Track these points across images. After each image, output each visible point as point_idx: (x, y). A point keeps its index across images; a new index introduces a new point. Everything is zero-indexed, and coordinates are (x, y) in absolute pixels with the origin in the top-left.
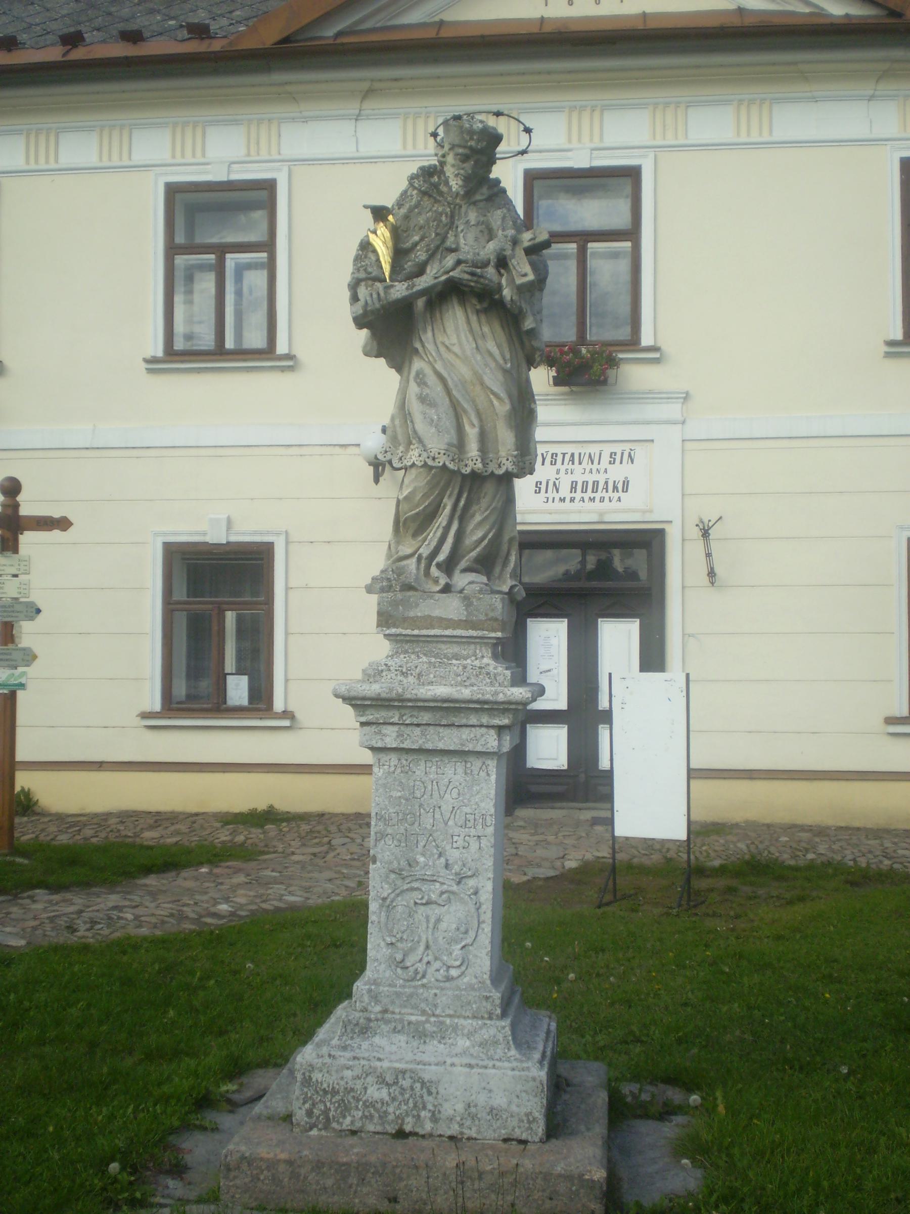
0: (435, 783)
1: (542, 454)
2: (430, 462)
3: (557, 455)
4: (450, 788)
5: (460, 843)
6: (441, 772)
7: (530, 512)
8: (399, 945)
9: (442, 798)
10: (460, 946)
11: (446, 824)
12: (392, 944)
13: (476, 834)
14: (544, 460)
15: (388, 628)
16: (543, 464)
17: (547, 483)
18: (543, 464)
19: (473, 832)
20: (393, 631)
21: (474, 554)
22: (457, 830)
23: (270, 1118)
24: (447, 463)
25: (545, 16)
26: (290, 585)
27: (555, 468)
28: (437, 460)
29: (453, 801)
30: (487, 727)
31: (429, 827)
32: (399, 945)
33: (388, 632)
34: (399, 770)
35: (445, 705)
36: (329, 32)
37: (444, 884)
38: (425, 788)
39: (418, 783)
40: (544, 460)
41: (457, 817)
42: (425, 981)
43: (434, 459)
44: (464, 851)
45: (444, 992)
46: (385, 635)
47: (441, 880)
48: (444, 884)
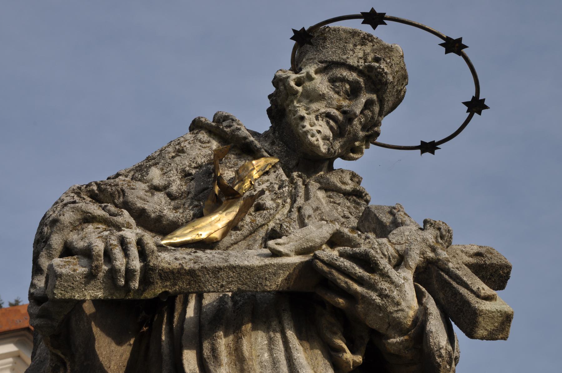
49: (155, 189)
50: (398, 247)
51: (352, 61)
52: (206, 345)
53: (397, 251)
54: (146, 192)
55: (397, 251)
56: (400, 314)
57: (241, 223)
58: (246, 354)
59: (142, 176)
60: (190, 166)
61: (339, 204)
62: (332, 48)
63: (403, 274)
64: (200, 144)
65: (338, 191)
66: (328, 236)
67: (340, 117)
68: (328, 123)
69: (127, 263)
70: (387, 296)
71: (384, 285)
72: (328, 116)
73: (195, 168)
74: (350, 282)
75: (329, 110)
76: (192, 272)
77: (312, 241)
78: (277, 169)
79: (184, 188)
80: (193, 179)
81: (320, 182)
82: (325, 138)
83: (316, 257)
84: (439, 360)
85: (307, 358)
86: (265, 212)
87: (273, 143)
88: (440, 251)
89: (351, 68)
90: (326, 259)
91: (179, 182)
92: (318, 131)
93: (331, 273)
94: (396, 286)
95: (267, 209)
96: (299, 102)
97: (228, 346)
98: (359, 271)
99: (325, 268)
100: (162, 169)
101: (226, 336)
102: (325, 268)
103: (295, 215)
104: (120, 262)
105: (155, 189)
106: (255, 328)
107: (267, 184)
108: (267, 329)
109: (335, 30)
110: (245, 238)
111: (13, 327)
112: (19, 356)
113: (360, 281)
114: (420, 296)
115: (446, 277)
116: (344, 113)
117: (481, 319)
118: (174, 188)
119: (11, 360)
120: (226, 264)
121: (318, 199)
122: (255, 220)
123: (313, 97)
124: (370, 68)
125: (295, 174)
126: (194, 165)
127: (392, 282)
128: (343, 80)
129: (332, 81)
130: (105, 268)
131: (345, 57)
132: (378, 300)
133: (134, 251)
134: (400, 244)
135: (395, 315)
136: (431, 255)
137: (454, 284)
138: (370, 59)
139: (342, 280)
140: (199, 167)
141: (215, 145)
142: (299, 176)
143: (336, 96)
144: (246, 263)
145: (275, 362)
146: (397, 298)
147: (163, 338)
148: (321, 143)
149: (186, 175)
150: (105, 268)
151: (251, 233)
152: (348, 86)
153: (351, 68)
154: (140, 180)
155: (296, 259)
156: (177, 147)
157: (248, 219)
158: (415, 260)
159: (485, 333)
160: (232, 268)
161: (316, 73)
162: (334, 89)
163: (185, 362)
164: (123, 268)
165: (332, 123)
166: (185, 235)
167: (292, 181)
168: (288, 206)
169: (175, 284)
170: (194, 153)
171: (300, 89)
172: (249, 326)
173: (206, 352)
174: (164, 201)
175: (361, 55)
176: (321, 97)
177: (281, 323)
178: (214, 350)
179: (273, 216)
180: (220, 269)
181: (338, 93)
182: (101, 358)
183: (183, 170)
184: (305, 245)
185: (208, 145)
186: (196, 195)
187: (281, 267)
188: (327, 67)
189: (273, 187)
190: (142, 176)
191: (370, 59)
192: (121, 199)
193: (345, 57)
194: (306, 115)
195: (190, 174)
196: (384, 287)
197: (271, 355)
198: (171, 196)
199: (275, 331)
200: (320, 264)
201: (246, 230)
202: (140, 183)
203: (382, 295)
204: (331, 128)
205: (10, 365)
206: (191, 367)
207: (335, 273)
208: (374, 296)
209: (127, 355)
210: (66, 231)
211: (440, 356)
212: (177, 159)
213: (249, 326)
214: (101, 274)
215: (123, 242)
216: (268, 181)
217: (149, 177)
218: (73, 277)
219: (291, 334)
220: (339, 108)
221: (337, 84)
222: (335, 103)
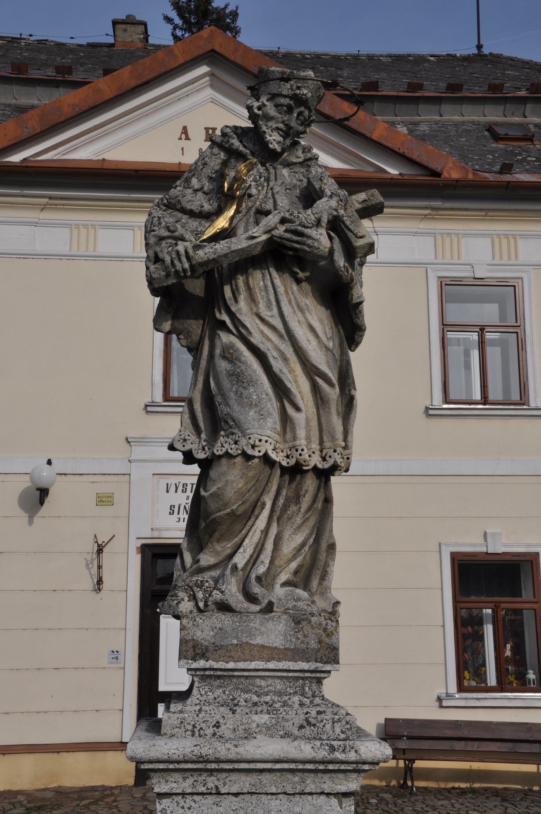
1: (176, 484)
2: (250, 452)
3: (187, 485)
7: (167, 529)
14: (177, 488)
15: (194, 659)
16: (176, 492)
17: (179, 507)
18: (176, 492)
20: (202, 663)
21: (294, 565)
24: (270, 452)
25: (182, 162)
27: (185, 495)
28: (257, 449)
30: (328, 794)
33: (195, 665)
35: (278, 766)
36: (16, 158)
40: (177, 488)
43: (253, 447)
46: (189, 670)
49: (196, 191)
50: (316, 216)
51: (285, 92)
52: (233, 282)
53: (316, 218)
54: (192, 194)
55: (316, 218)
56: (321, 253)
57: (240, 209)
58: (252, 286)
59: (188, 185)
60: (211, 173)
61: (296, 173)
62: (273, 84)
63: (320, 231)
64: (214, 157)
65: (295, 164)
66: (278, 221)
67: (284, 129)
68: (279, 133)
69: (182, 266)
70: (312, 247)
71: (310, 242)
72: (277, 128)
73: (214, 173)
74: (293, 244)
75: (277, 125)
76: (214, 260)
77: (270, 226)
78: (257, 165)
79: (211, 187)
80: (214, 180)
81: (283, 165)
82: (279, 143)
83: (273, 236)
84: (341, 273)
85: (281, 281)
86: (252, 198)
87: (254, 144)
88: (339, 211)
89: (285, 96)
90: (278, 235)
91: (207, 184)
92: (274, 140)
93: (282, 242)
94: (316, 240)
95: (253, 196)
96: (262, 121)
97: (243, 281)
98: (295, 238)
99: (279, 240)
100: (198, 178)
101: (242, 276)
102: (279, 240)
103: (270, 195)
104: (179, 267)
105: (196, 191)
106: (255, 269)
107: (253, 177)
108: (261, 268)
109: (272, 72)
110: (244, 216)
111: (202, 52)
112: (213, 74)
113: (297, 242)
114: (331, 238)
115: (343, 226)
116: (286, 125)
117: (357, 250)
118: (206, 188)
119: (207, 78)
120: (229, 251)
121: (284, 176)
122: (248, 205)
123: (268, 118)
124: (295, 95)
125: (268, 165)
126: (213, 171)
127: (313, 239)
128: (282, 105)
129: (276, 106)
130: (173, 270)
131: (280, 90)
132: (308, 249)
133: (184, 259)
134: (317, 213)
135: (318, 253)
136: (335, 213)
137: (346, 230)
138: (294, 88)
139: (288, 243)
140: (217, 172)
141: (222, 155)
142: (270, 165)
143: (280, 115)
144: (240, 247)
145: (266, 286)
146: (317, 246)
147: (216, 276)
148: (277, 146)
149: (210, 178)
150: (173, 270)
151: (247, 212)
152: (285, 108)
153: (285, 96)
154: (188, 188)
155: (264, 237)
156: (203, 162)
157: (244, 205)
158: (325, 220)
159: (362, 255)
160: (233, 252)
161: (267, 100)
162: (278, 112)
163: (225, 293)
164: (181, 269)
165: (280, 132)
166: (210, 232)
167: (267, 169)
168: (265, 188)
169: (207, 267)
170: (212, 164)
171: (260, 112)
172: (251, 269)
173: (234, 287)
174: (202, 197)
175: (289, 87)
176: (271, 118)
177: (267, 263)
178: (236, 286)
179: (258, 198)
180: (227, 254)
181: (280, 113)
182: (190, 291)
183: (209, 176)
184: (267, 229)
185: (219, 156)
186: (217, 191)
187: (258, 243)
188: (273, 97)
189: (256, 178)
190: (188, 185)
191: (294, 88)
192: (180, 206)
193: (280, 90)
194: (266, 130)
195: (213, 178)
196: (309, 243)
197: (264, 283)
198: (204, 193)
199: (264, 269)
200: (276, 238)
201: (244, 211)
202: (188, 190)
203: (309, 246)
204: (281, 136)
205: (209, 82)
206: (228, 295)
207: (284, 241)
208: (306, 248)
209: (203, 282)
210: (153, 248)
211: (341, 271)
212: (204, 170)
213: (251, 269)
214: (172, 273)
215: (178, 253)
216: (253, 174)
217: (192, 184)
218: (160, 278)
219: (272, 270)
220: (283, 122)
221: (279, 108)
222: (280, 120)
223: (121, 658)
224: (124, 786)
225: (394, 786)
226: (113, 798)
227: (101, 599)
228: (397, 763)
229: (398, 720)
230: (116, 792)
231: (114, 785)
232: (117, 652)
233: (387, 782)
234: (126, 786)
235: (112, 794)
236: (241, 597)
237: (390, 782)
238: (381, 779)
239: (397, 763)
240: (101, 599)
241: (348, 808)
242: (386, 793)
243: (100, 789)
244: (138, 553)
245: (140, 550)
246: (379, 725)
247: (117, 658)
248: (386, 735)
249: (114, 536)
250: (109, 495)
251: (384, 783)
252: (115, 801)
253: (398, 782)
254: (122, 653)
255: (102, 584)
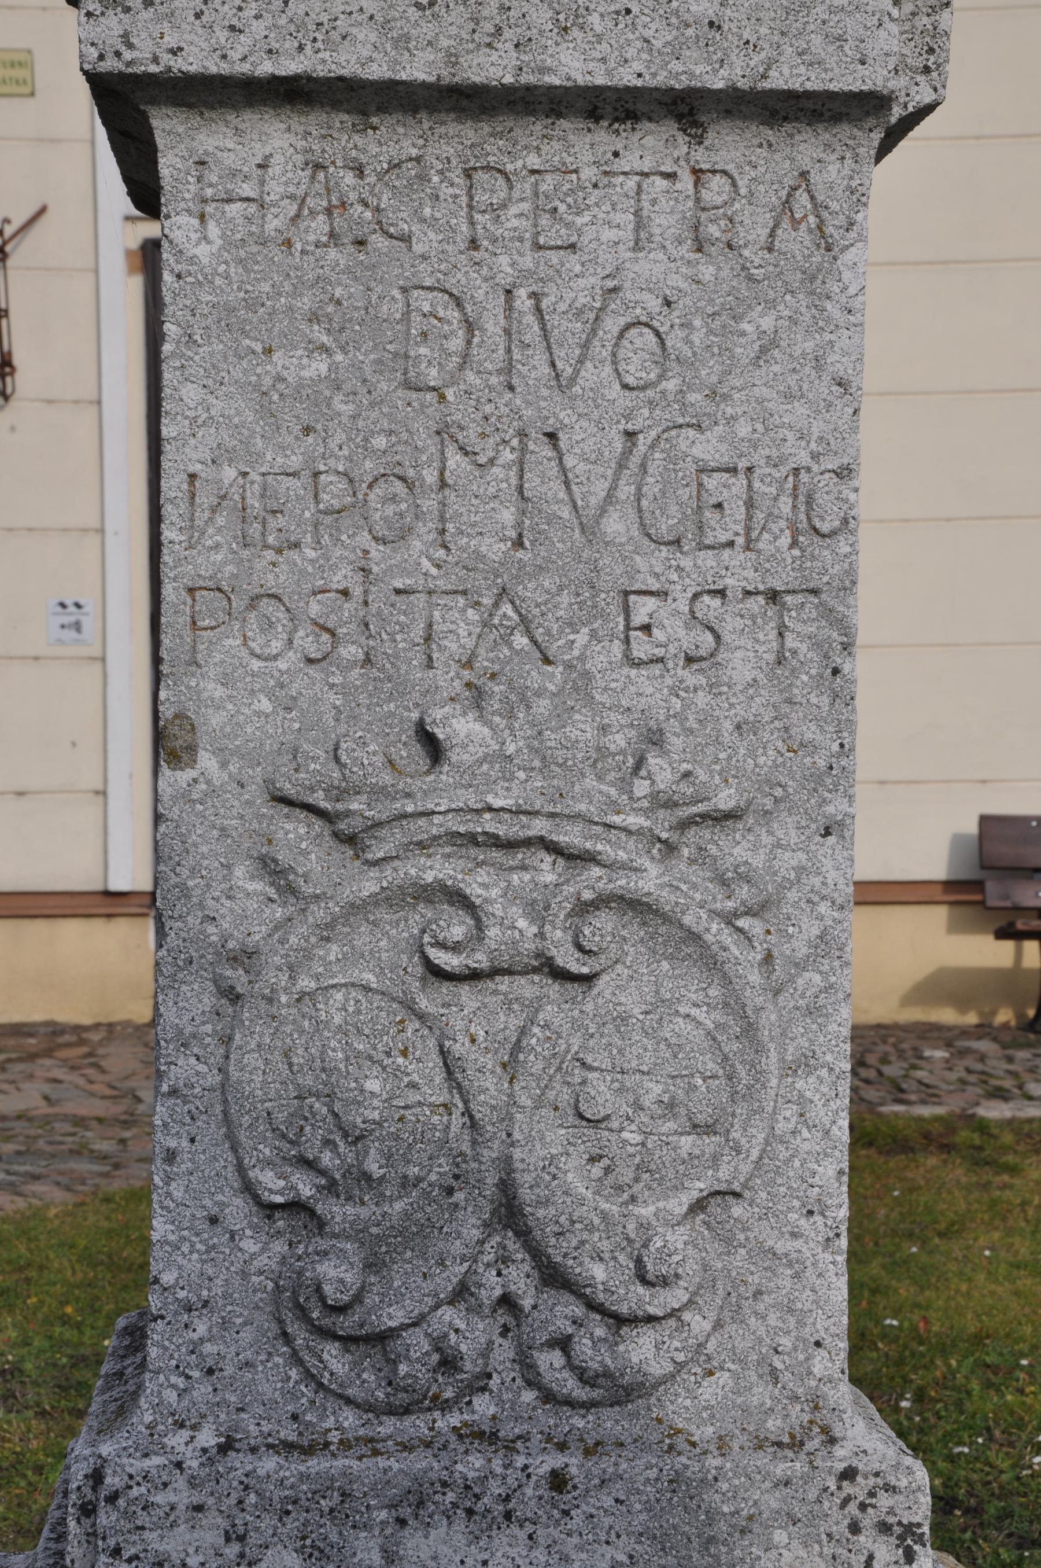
0: (523, 301)
4: (612, 325)
5: (675, 633)
6: (565, 236)
8: (338, 1212)
9: (561, 383)
10: (679, 1204)
11: (589, 529)
12: (295, 1206)
13: (752, 579)
19: (739, 571)
22: (651, 565)
23: (156, 1003)
26: (97, 667)
29: (625, 400)
31: (494, 549)
32: (338, 1212)
34: (319, 226)
37: (589, 858)
38: (470, 326)
39: (424, 301)
41: (652, 487)
42: (483, 1406)
44: (691, 678)
45: (606, 1464)
47: (570, 836)
48: (589, 858)
223: (89, 624)
224: (119, 1023)
225: (1005, 1026)
226: (85, 1050)
227: (13, 429)
228: (1019, 955)
229: (1025, 820)
230: (95, 1037)
231: (86, 1021)
232: (78, 605)
233: (981, 1014)
234: (127, 1024)
235: (82, 1042)
236: (474, 891)
237: (994, 1013)
238: (962, 1004)
239: (1019, 955)
240: (13, 429)
241: (925, 20)
242: (979, 1038)
243: (42, 1030)
244: (131, 271)
245: (138, 261)
246: (958, 841)
247: (77, 626)
248: (983, 867)
249: (43, 210)
250: (16, 57)
251: (972, 1019)
252: (90, 1055)
253: (1020, 1015)
254: (91, 605)
255: (12, 374)
